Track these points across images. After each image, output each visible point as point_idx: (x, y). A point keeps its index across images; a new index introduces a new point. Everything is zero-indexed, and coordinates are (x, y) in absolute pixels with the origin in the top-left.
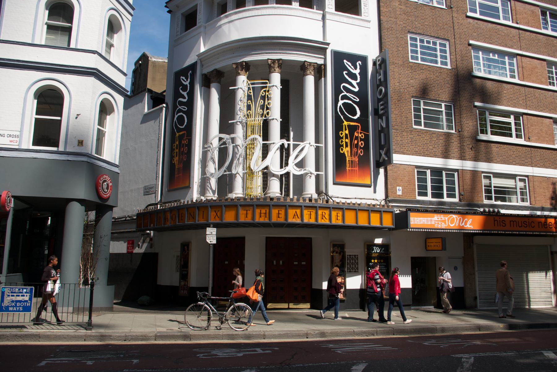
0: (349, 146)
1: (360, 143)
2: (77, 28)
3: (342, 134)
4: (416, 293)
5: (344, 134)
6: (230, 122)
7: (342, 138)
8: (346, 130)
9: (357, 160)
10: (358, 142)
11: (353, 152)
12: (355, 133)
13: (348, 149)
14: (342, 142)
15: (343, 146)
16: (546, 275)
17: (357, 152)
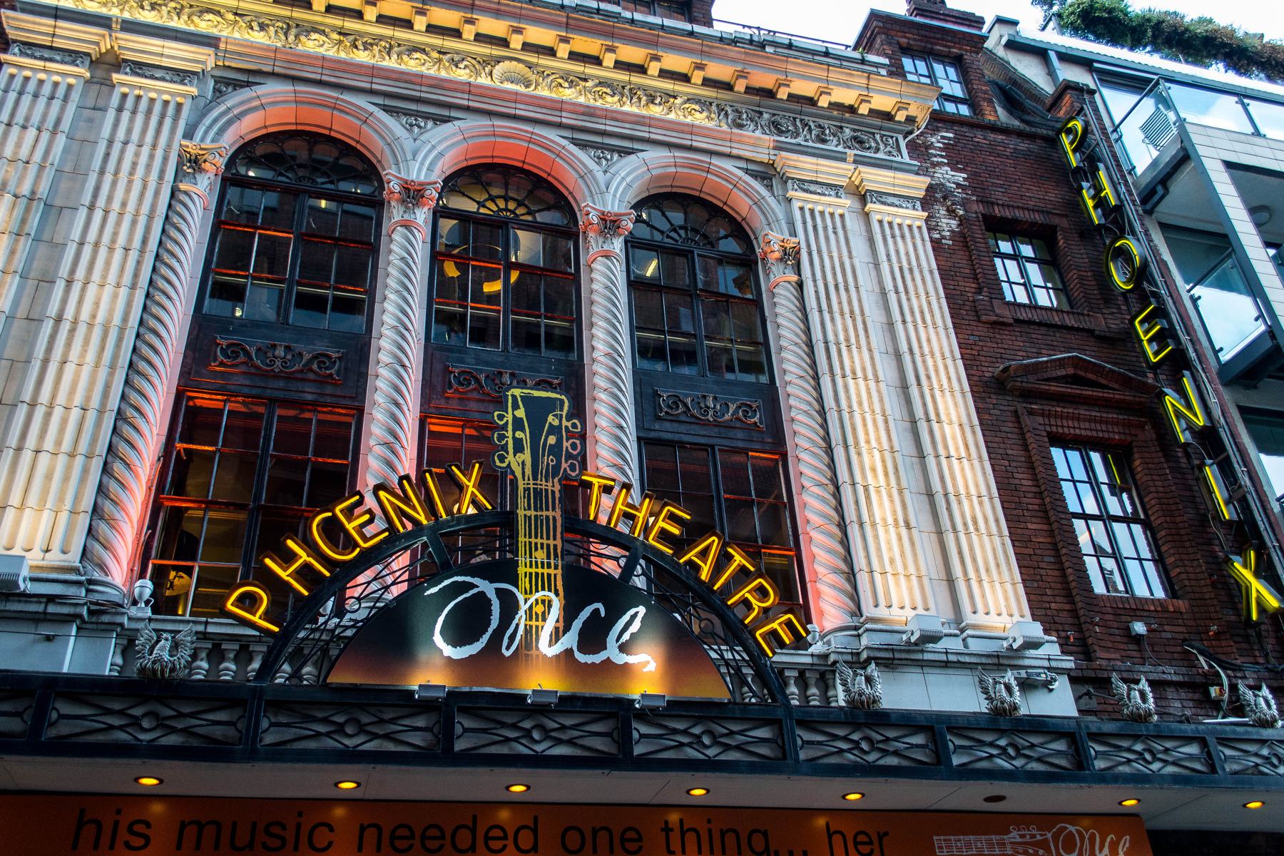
0: (528, 451)
1: (566, 444)
2: (48, 585)
3: (501, 417)
4: (330, 604)
5: (509, 417)
6: (306, 593)
7: (505, 427)
8: (516, 407)
9: (557, 488)
10: (559, 441)
11: (542, 467)
12: (550, 418)
13: (526, 456)
14: (502, 437)
15: (505, 448)
16: (708, 220)
17: (557, 468)
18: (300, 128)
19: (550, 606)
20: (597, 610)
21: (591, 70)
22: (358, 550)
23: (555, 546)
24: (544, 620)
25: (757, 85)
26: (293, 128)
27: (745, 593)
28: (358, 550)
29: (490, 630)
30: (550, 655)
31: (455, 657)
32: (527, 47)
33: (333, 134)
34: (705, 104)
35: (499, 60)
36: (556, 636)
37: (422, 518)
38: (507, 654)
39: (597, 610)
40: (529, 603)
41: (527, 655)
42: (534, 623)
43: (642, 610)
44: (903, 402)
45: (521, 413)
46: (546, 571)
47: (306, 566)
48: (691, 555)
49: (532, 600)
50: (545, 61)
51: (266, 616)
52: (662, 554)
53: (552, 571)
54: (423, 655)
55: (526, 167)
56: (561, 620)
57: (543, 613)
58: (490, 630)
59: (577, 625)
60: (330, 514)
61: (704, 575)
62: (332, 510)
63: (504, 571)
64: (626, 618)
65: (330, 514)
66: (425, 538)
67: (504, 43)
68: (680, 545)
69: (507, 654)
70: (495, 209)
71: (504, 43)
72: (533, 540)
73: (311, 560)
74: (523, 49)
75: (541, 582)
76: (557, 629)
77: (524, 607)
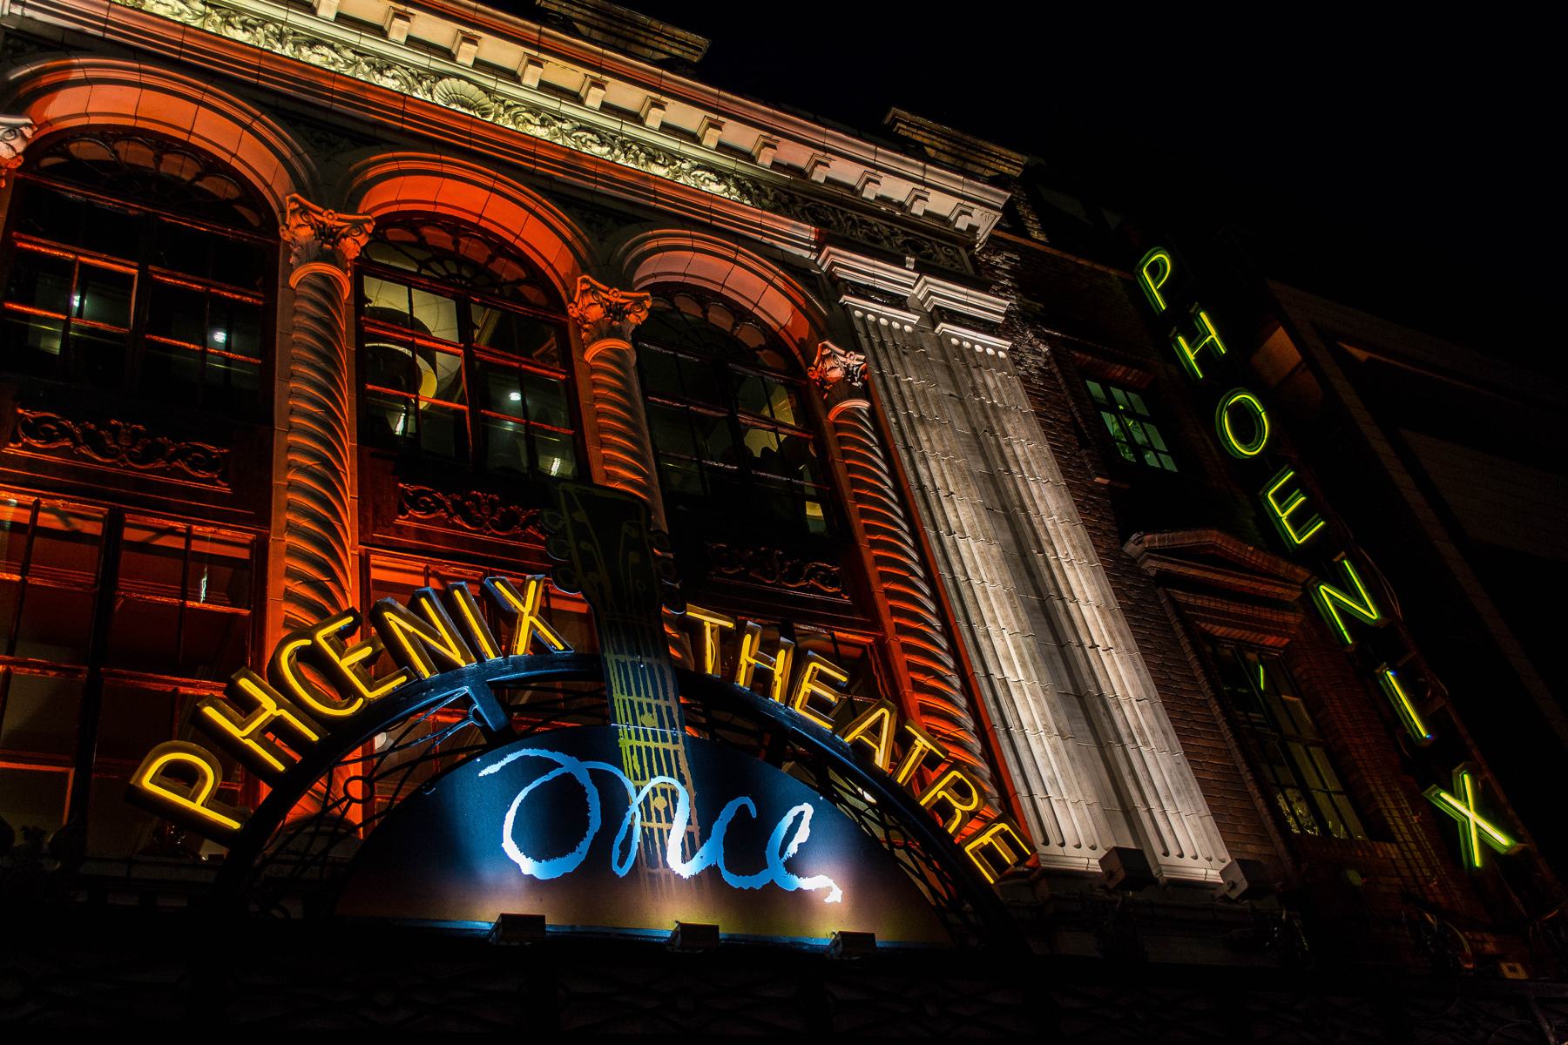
12: (625, 528)
18: (141, 124)
19: (675, 799)
20: (743, 809)
21: (567, 109)
22: (360, 701)
23: (669, 709)
24: (670, 820)
25: (785, 160)
26: (130, 122)
27: (938, 792)
28: (360, 701)
29: (590, 835)
30: (686, 875)
31: (539, 876)
32: (479, 64)
33: (194, 140)
34: (722, 175)
35: (441, 76)
36: (690, 848)
37: (455, 655)
38: (622, 872)
39: (743, 809)
40: (643, 793)
41: (651, 875)
42: (654, 824)
43: (808, 809)
44: (1024, 573)
45: (581, 516)
46: (661, 745)
47: (277, 726)
48: (856, 734)
49: (647, 789)
50: (504, 87)
51: (215, 801)
52: (818, 731)
53: (670, 746)
54: (489, 872)
55: (483, 224)
56: (695, 821)
57: (667, 809)
58: (590, 835)
59: (719, 828)
60: (308, 642)
61: (881, 759)
62: (311, 636)
63: (596, 740)
64: (788, 820)
65: (308, 642)
66: (466, 689)
67: (448, 55)
68: (846, 715)
69: (622, 872)
70: (444, 273)
71: (448, 55)
72: (635, 698)
73: (284, 713)
74: (474, 67)
75: (656, 763)
76: (689, 834)
77: (637, 801)
